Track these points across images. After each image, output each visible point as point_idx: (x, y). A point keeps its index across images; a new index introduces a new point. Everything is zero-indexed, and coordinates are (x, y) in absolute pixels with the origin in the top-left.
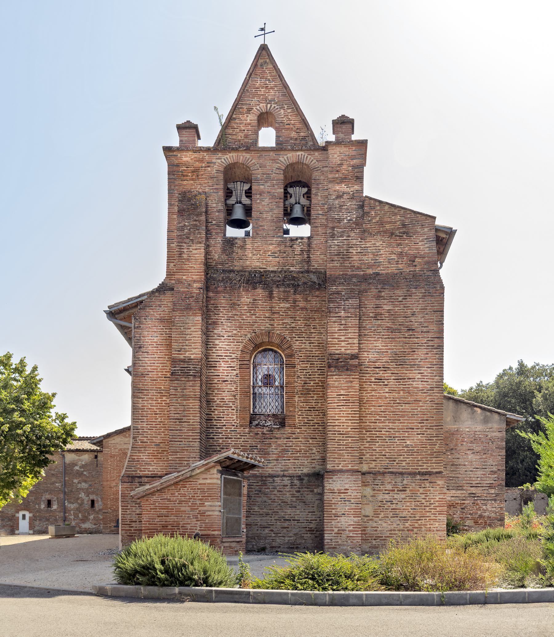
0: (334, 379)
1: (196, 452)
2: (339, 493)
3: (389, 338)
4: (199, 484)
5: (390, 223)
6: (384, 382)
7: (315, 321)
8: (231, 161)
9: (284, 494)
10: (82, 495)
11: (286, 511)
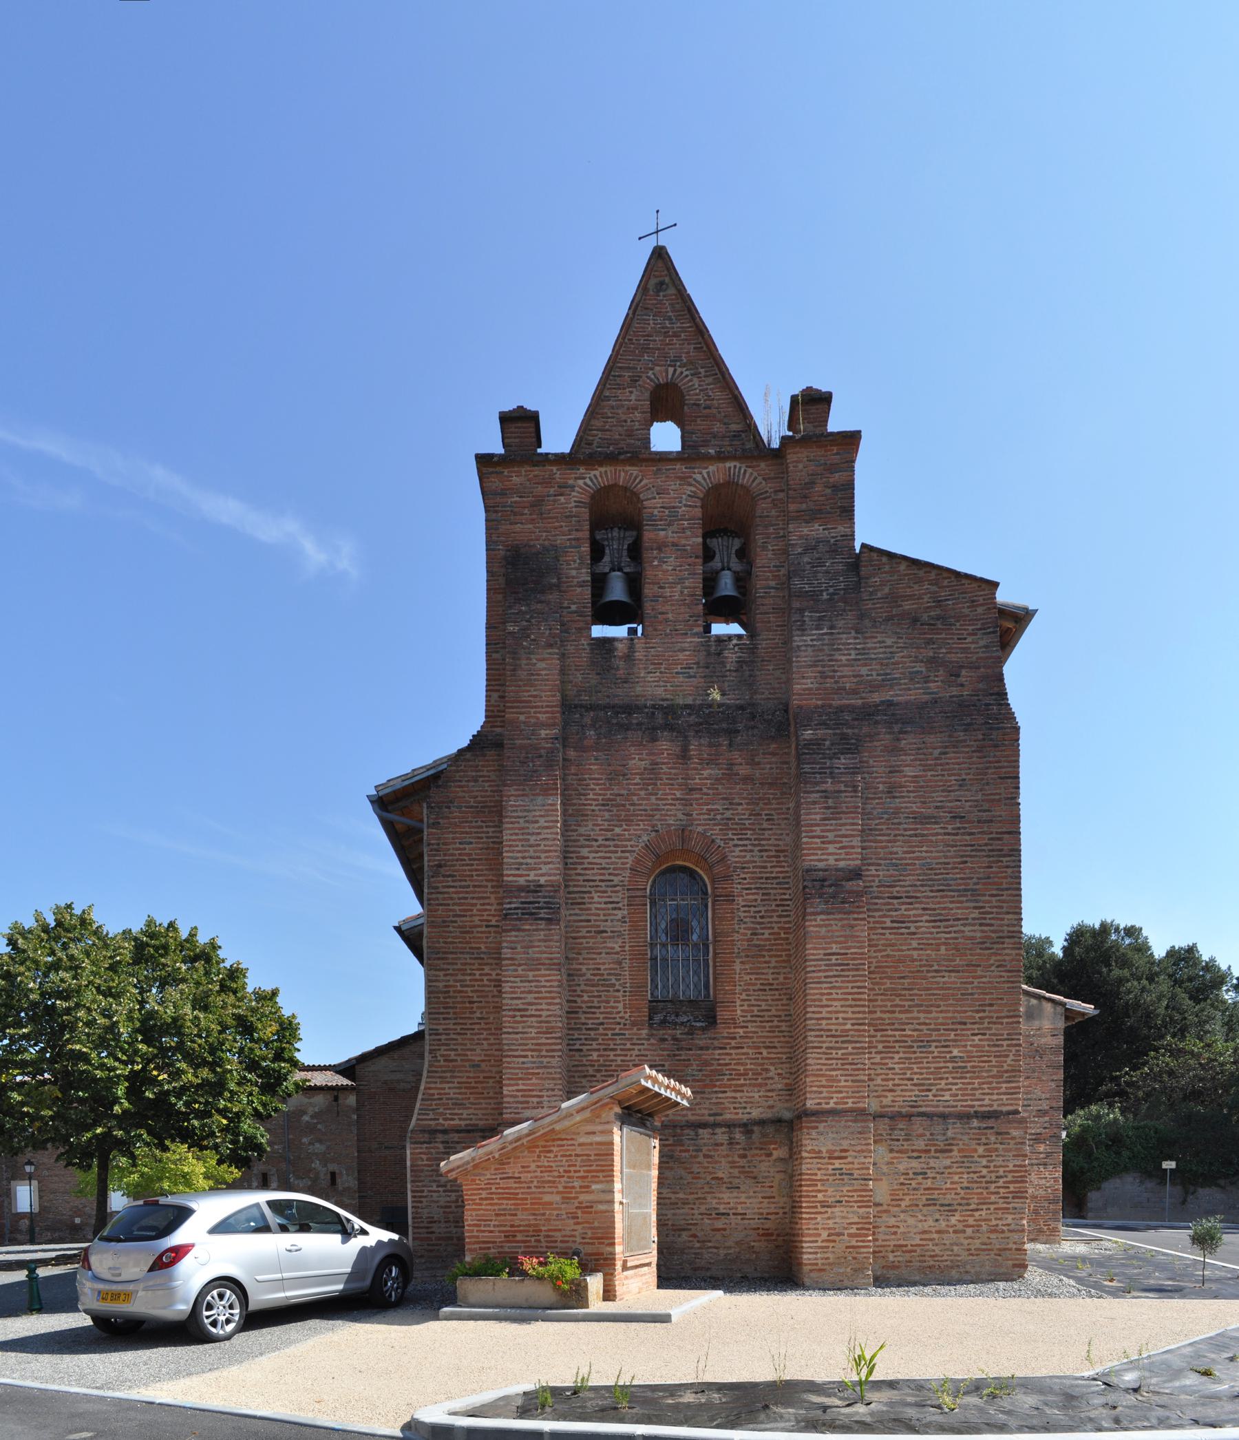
0: (819, 922)
1: (554, 1079)
2: (830, 1158)
3: (916, 835)
4: (580, 1145)
5: (911, 597)
6: (909, 928)
7: (770, 804)
8: (603, 482)
9: (716, 1162)
10: (316, 1164)
11: (721, 1195)
